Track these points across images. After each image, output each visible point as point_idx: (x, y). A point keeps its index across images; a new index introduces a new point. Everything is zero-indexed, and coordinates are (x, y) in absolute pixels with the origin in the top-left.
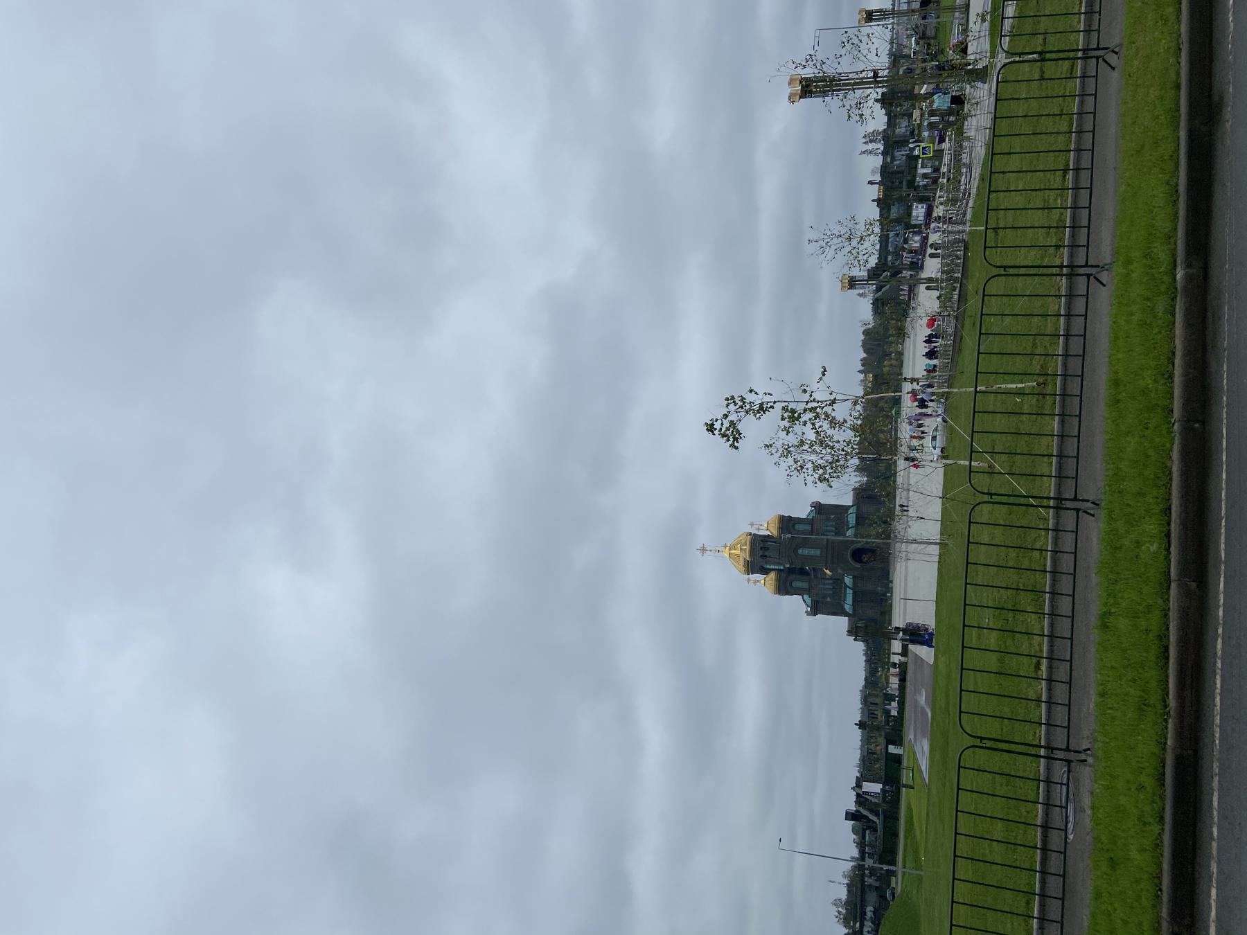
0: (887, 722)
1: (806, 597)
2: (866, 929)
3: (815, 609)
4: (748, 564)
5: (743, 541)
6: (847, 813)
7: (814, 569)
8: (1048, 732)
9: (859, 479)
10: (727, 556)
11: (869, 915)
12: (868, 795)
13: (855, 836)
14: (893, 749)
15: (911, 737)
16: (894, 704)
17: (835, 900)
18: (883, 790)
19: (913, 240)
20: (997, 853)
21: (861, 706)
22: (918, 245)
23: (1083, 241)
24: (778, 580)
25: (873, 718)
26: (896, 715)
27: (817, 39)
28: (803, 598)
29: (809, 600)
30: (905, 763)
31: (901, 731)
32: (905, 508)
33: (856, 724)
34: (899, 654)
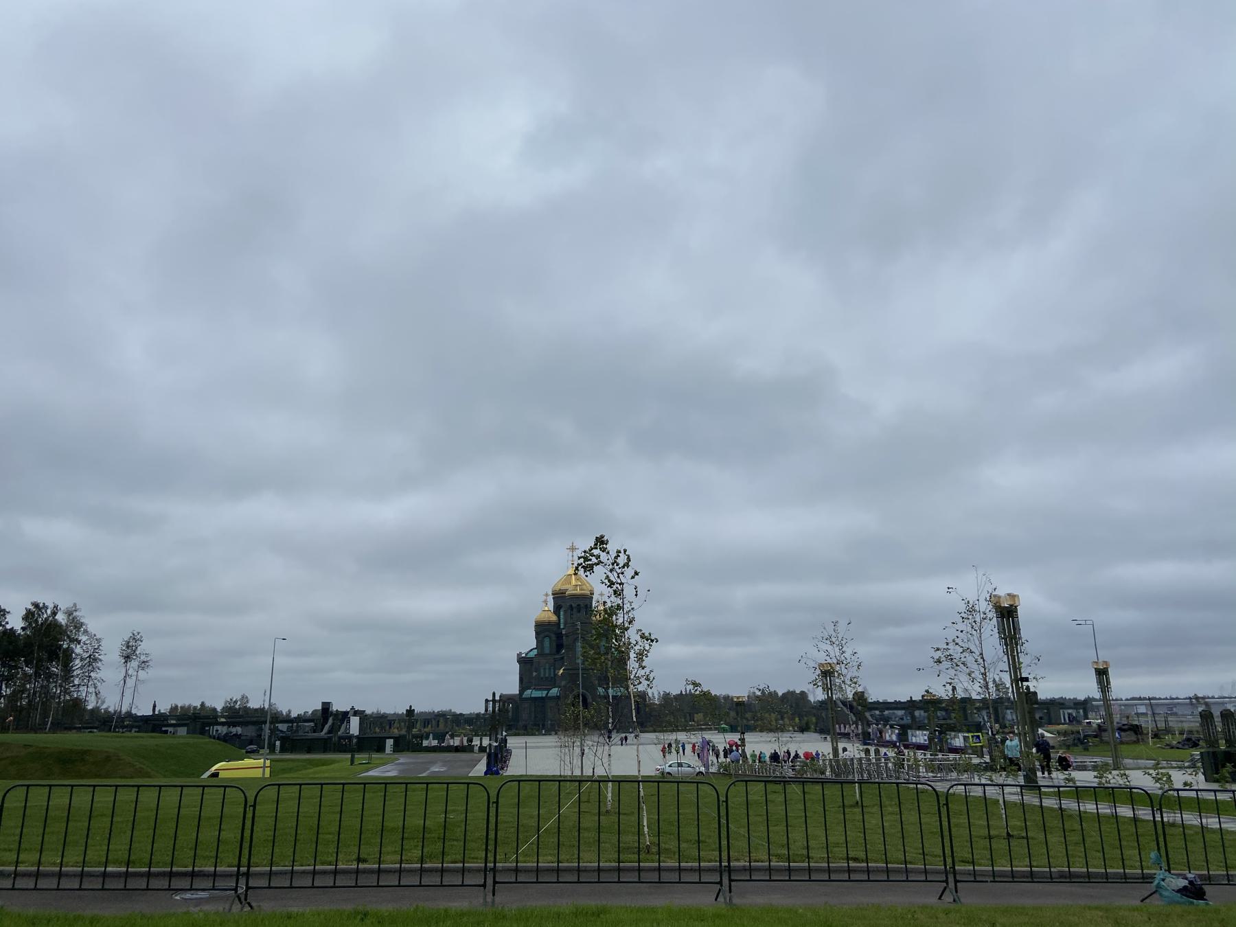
0: (415, 737)
1: (535, 652)
2: (219, 728)
3: (524, 661)
4: (562, 593)
5: (584, 587)
6: (329, 703)
7: (562, 658)
8: (285, 873)
9: (657, 697)
10: (569, 573)
11: (234, 730)
12: (347, 723)
13: (310, 713)
14: (390, 743)
15: (402, 760)
16: (435, 743)
17: (247, 697)
18: (350, 737)
19: (892, 734)
20: (208, 834)
21: (436, 711)
22: (888, 738)
23: (853, 877)
24: (549, 623)
25: (425, 724)
26: (424, 745)
27: (1083, 622)
28: (534, 649)
29: (532, 654)
30: (375, 756)
31: (408, 750)
32: (624, 742)
33: (411, 707)
34: (481, 744)
